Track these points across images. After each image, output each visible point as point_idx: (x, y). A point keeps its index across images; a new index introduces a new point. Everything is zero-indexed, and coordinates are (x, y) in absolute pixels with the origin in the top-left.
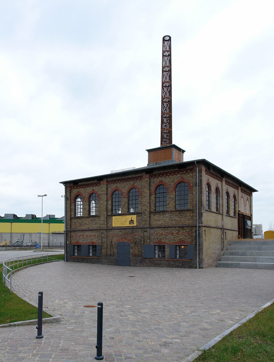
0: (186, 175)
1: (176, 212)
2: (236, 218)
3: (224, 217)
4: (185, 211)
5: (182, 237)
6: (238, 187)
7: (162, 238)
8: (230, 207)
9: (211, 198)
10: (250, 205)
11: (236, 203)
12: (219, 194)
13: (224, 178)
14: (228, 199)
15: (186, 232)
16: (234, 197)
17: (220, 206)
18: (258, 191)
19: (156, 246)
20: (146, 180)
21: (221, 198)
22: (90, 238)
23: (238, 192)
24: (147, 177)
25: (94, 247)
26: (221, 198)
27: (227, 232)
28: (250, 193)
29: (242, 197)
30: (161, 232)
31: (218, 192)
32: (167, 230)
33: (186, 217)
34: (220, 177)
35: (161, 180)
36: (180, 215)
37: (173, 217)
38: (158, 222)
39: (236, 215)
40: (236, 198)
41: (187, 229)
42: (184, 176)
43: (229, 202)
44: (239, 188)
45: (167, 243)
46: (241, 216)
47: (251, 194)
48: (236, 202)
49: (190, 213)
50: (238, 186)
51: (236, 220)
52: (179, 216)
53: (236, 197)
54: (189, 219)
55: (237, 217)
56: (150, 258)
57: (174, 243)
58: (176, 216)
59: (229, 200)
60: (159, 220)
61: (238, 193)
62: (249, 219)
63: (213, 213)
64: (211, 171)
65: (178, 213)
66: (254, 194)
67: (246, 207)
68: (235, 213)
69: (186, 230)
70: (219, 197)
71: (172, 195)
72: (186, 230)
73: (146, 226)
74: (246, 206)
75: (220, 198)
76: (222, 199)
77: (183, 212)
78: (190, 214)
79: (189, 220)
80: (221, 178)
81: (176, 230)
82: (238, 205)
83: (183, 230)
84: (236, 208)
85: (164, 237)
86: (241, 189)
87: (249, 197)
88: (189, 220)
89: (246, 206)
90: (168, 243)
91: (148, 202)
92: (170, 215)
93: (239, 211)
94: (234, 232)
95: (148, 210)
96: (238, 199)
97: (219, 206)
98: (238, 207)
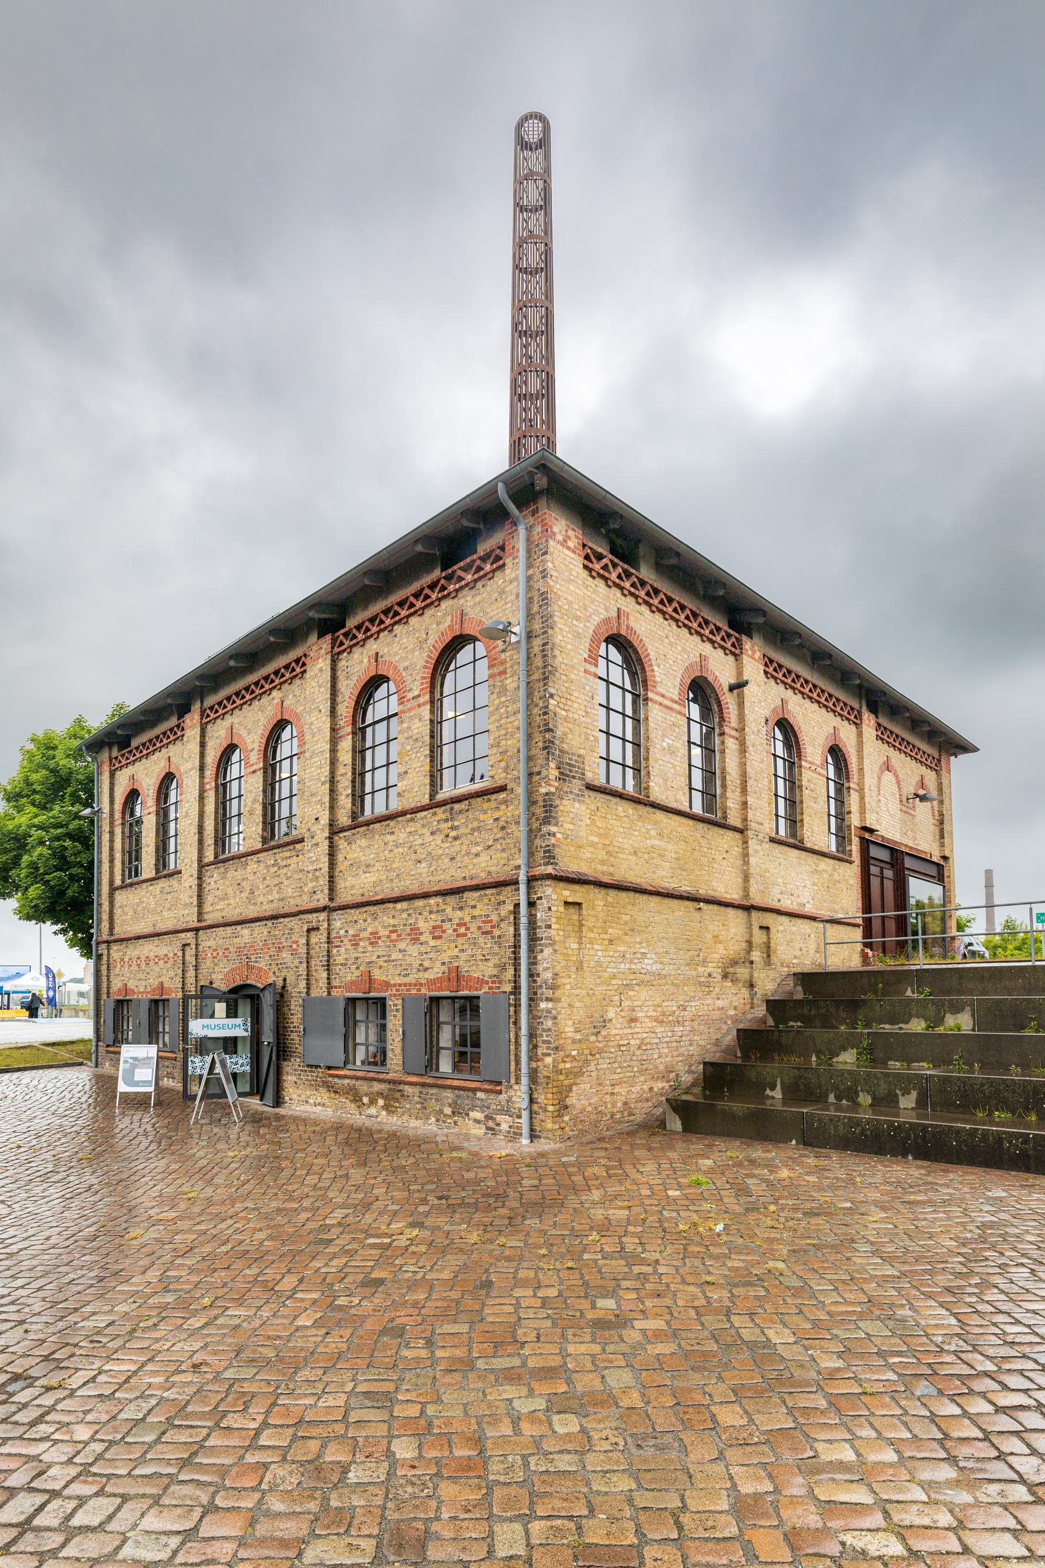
0: (476, 595)
1: (435, 814)
2: (851, 862)
3: (753, 844)
4: (473, 801)
5: (456, 952)
6: (860, 712)
7: (374, 958)
8: (802, 802)
9: (647, 724)
10: (936, 813)
11: (849, 788)
12: (722, 719)
13: (758, 640)
14: (794, 763)
15: (474, 917)
16: (836, 752)
17: (724, 786)
18: (975, 749)
19: (358, 1003)
20: (321, 670)
21: (731, 744)
22: (157, 969)
23: (860, 734)
24: (323, 652)
25: (469, 1006)
26: (731, 744)
27: (780, 926)
28: (936, 756)
29: (887, 767)
30: (370, 930)
31: (715, 707)
32: (393, 917)
33: (476, 834)
34: (726, 628)
35: (377, 654)
36: (450, 824)
37: (420, 841)
38: (363, 876)
39: (848, 848)
40: (846, 766)
41: (480, 899)
42: (467, 601)
43: (801, 775)
44: (867, 716)
45: (395, 985)
46: (884, 855)
47: (939, 761)
48: (846, 785)
49: (497, 808)
50: (856, 706)
51: (850, 874)
52: (446, 832)
53: (845, 760)
54: (490, 843)
55: (856, 856)
56: (329, 1068)
57: (421, 985)
58: (432, 834)
59: (800, 766)
60: (368, 866)
61: (860, 744)
62: (934, 873)
63: (660, 815)
64: (646, 572)
65: (444, 816)
66: (958, 763)
67: (914, 816)
68: (842, 837)
69: (474, 907)
70: (722, 734)
71: (417, 720)
72: (474, 907)
73: (318, 900)
74: (912, 812)
75: (723, 743)
76: (743, 750)
77: (463, 807)
78: (496, 815)
79: (489, 847)
80: (729, 636)
81: (431, 912)
82: (862, 798)
83: (461, 908)
84: (849, 813)
85: (380, 953)
86: (879, 725)
87: (930, 776)
88: (489, 847)
89: (912, 812)
90: (400, 985)
91: (323, 779)
92: (408, 830)
93: (865, 829)
94: (835, 933)
95: (325, 819)
96: (861, 770)
97: (718, 783)
98: (862, 811)
